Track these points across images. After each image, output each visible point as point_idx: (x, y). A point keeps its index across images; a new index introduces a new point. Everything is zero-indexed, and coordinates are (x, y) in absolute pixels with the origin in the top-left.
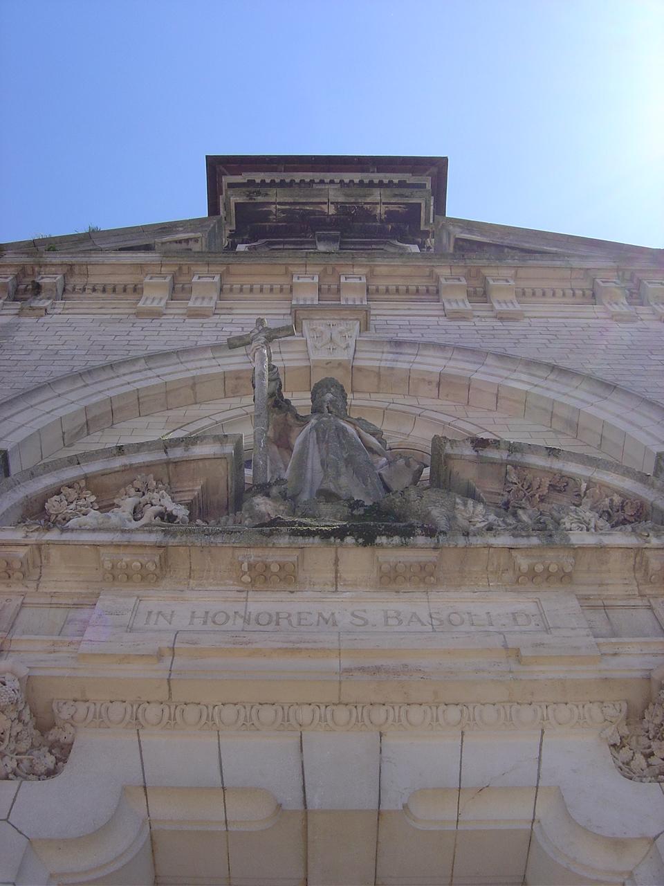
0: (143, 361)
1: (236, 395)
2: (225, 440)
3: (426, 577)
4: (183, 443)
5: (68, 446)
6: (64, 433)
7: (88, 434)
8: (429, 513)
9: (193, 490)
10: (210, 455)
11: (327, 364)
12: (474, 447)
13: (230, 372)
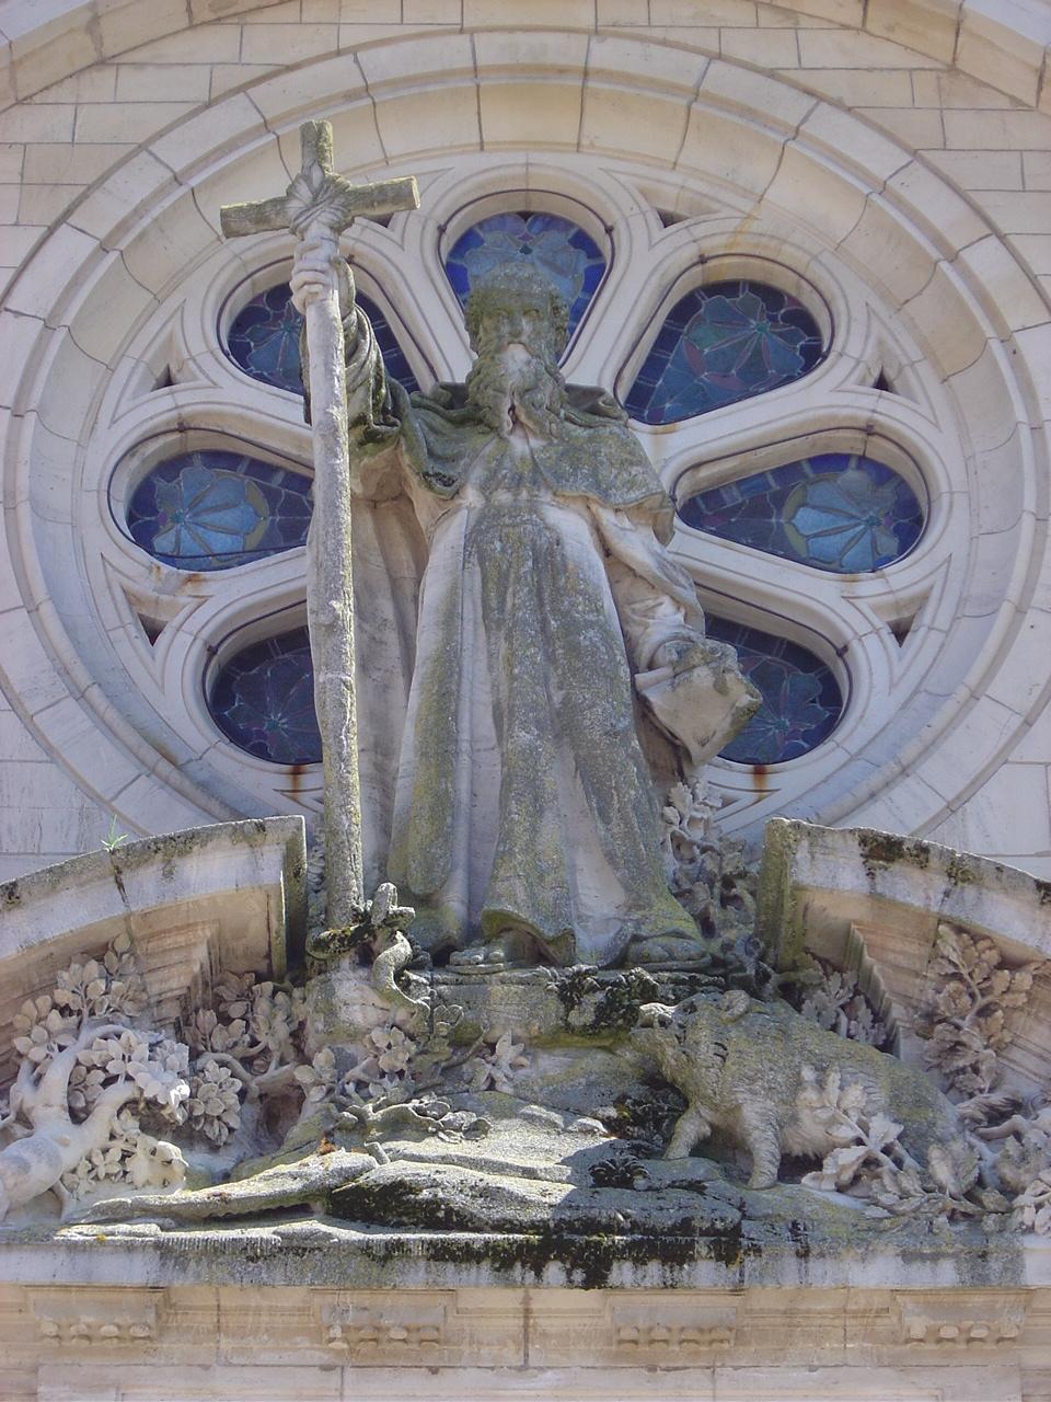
2: (259, 837)
4: (159, 856)
8: (738, 1107)
12: (867, 857)
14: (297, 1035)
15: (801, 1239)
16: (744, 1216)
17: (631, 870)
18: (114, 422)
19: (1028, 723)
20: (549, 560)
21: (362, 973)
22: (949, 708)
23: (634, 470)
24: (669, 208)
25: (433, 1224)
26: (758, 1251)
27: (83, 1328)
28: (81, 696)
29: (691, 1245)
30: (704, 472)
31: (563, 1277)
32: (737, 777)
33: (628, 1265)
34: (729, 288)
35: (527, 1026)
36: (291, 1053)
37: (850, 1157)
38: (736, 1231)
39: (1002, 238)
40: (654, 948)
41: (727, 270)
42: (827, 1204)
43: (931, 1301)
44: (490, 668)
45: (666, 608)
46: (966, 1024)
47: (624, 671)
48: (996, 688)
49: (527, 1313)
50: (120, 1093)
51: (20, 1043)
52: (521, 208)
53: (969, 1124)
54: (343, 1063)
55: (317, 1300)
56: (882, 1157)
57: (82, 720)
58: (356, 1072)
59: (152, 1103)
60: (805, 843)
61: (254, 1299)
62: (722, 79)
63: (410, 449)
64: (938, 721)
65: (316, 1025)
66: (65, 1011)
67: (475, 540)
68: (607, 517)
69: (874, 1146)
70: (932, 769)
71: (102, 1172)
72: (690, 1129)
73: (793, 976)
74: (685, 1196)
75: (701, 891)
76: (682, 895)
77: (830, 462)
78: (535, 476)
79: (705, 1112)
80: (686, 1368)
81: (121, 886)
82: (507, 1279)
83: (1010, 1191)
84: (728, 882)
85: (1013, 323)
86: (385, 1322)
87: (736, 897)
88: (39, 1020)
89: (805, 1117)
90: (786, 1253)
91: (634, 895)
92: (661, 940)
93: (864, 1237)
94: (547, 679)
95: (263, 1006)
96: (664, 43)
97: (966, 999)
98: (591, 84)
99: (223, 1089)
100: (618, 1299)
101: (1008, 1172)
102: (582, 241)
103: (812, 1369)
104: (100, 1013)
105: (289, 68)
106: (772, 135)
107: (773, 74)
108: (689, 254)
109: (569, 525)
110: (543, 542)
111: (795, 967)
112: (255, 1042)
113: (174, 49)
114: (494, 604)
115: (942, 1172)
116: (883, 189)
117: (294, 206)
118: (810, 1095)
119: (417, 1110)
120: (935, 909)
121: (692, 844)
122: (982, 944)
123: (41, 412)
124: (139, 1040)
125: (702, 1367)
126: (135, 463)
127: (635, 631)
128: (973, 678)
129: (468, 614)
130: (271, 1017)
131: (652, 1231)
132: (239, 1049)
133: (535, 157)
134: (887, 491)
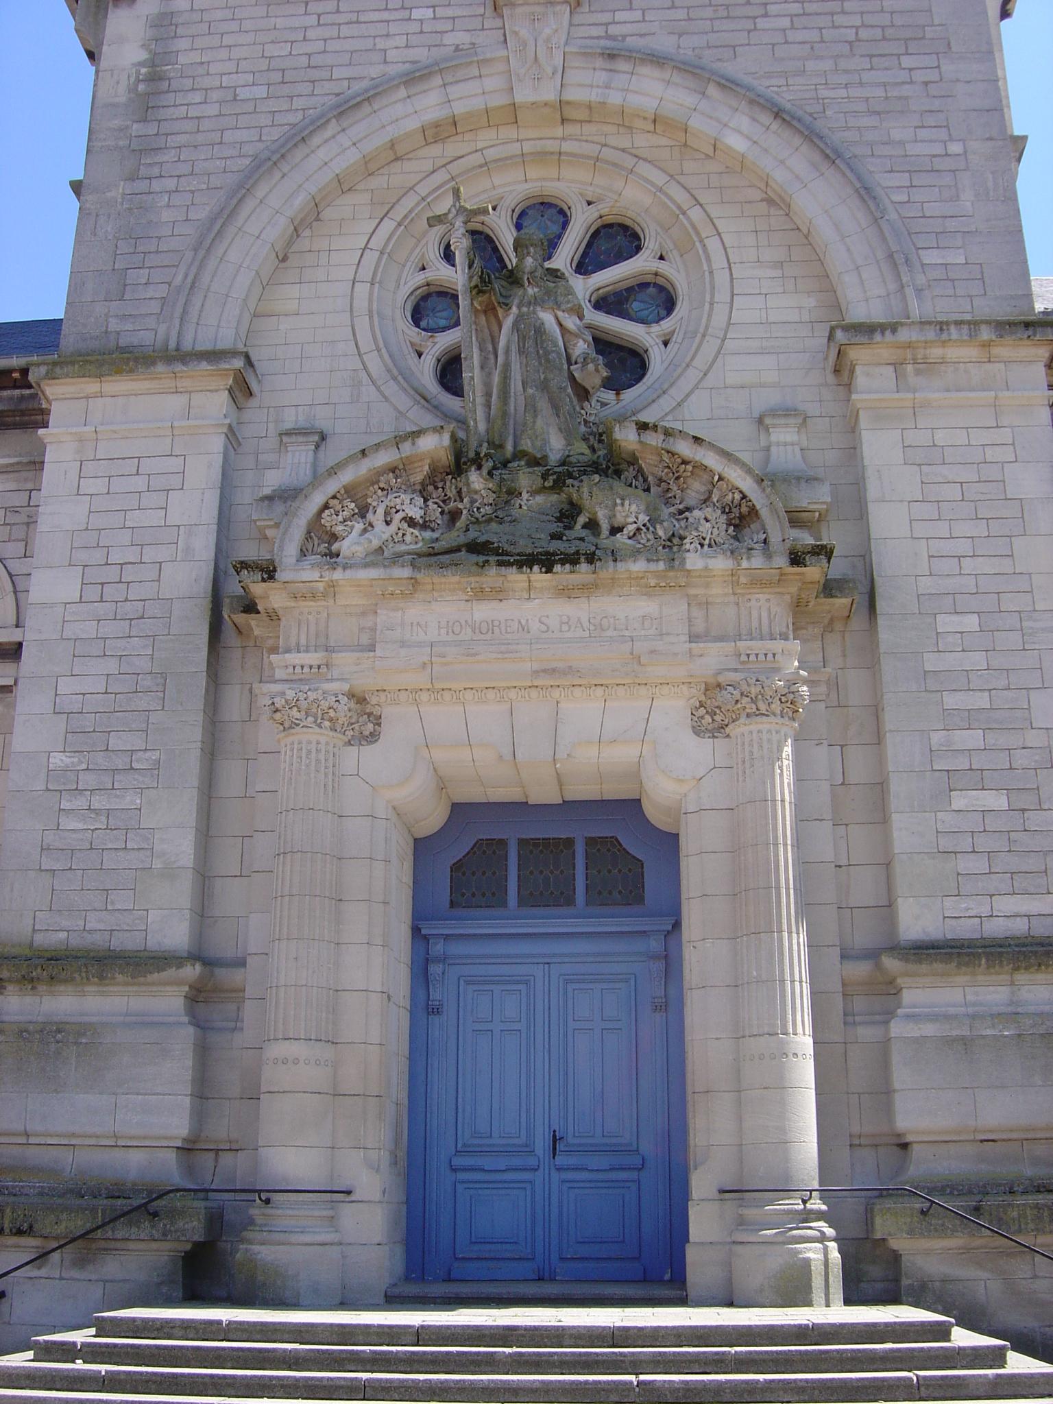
0: (334, 120)
3: (587, 590)
12: (638, 429)
14: (459, 492)
15: (615, 556)
16: (597, 549)
17: (568, 433)
18: (405, 284)
19: (705, 375)
20: (540, 330)
21: (478, 472)
22: (679, 370)
23: (570, 297)
24: (590, 199)
25: (498, 554)
26: (600, 560)
27: (390, 592)
28: (395, 379)
29: (579, 559)
30: (601, 291)
31: (539, 570)
32: (609, 396)
33: (559, 566)
34: (611, 226)
35: (532, 487)
36: (458, 499)
37: (632, 528)
38: (594, 553)
39: (701, 205)
40: (573, 459)
41: (609, 219)
42: (624, 543)
43: (656, 574)
44: (521, 368)
45: (581, 343)
46: (671, 482)
47: (565, 366)
48: (695, 363)
49: (530, 581)
50: (401, 515)
51: (369, 500)
52: (541, 201)
53: (672, 515)
54: (473, 502)
55: (463, 580)
56: (643, 528)
57: (396, 388)
58: (477, 504)
59: (411, 518)
60: (618, 425)
61: (443, 580)
62: (607, 153)
63: (494, 294)
64: (676, 374)
65: (464, 489)
66: (383, 489)
67: (516, 324)
68: (560, 314)
69: (640, 524)
70: (672, 391)
71: (396, 540)
72: (582, 520)
73: (617, 467)
74: (578, 542)
75: (591, 438)
76: (585, 439)
77: (644, 285)
78: (535, 301)
79: (587, 515)
81: (398, 449)
83: (682, 538)
84: (601, 435)
85: (704, 236)
86: (484, 586)
87: (603, 440)
88: (375, 492)
89: (618, 515)
92: (576, 457)
93: (635, 554)
94: (539, 371)
95: (448, 483)
96: (587, 141)
97: (671, 474)
98: (562, 158)
99: (434, 511)
100: (556, 576)
101: (681, 532)
102: (561, 212)
103: (620, 596)
104: (394, 489)
105: (463, 157)
106: (623, 173)
107: (623, 150)
108: (596, 215)
109: (547, 318)
110: (537, 324)
111: (619, 464)
112: (446, 495)
113: (420, 153)
114: (521, 346)
115: (660, 532)
116: (661, 190)
117: (451, 216)
118: (619, 508)
119: (496, 516)
120: (660, 445)
121: (590, 422)
122: (676, 456)
123: (380, 283)
124: (406, 498)
126: (413, 297)
127: (571, 351)
128: (688, 360)
129: (514, 350)
130: (450, 487)
131: (567, 554)
132: (441, 498)
133: (544, 184)
134: (663, 295)
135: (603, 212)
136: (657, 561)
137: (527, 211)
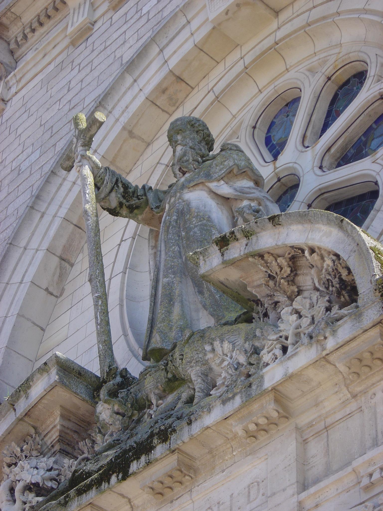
1: (177, 105)
2: (47, 367)
4: (22, 393)
5: (61, 295)
6: (47, 290)
7: (72, 265)
9: (55, 426)
10: (42, 393)
11: (227, 13)
13: (152, 92)
30: (333, 150)
60: (201, 258)
80: (183, 495)
82: (100, 490)
90: (184, 426)
91: (216, 317)
100: (139, 477)
108: (323, 79)
118: (210, 356)
125: (187, 492)
135: (329, 73)
136: (233, 397)
137: (275, 120)
